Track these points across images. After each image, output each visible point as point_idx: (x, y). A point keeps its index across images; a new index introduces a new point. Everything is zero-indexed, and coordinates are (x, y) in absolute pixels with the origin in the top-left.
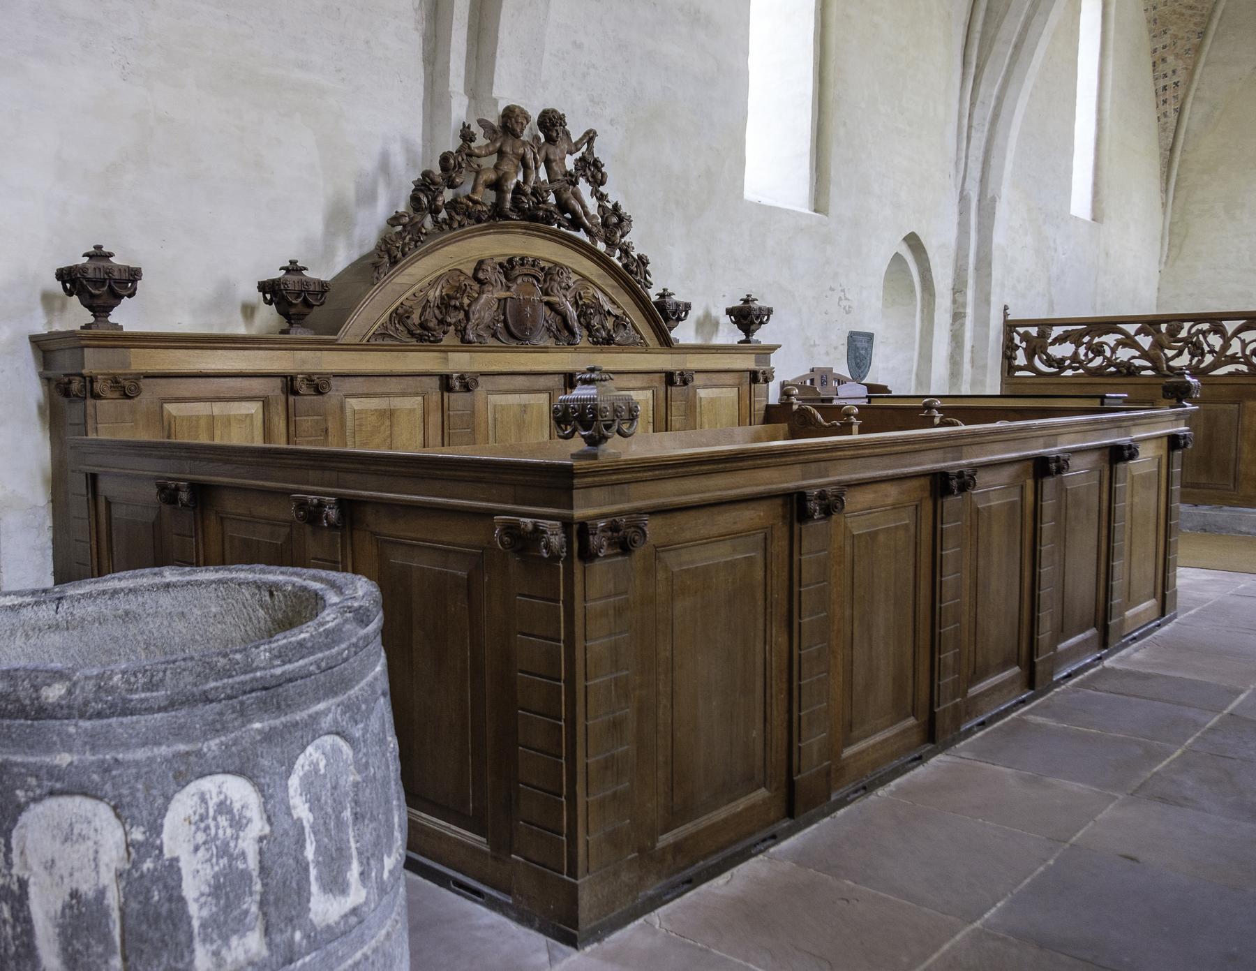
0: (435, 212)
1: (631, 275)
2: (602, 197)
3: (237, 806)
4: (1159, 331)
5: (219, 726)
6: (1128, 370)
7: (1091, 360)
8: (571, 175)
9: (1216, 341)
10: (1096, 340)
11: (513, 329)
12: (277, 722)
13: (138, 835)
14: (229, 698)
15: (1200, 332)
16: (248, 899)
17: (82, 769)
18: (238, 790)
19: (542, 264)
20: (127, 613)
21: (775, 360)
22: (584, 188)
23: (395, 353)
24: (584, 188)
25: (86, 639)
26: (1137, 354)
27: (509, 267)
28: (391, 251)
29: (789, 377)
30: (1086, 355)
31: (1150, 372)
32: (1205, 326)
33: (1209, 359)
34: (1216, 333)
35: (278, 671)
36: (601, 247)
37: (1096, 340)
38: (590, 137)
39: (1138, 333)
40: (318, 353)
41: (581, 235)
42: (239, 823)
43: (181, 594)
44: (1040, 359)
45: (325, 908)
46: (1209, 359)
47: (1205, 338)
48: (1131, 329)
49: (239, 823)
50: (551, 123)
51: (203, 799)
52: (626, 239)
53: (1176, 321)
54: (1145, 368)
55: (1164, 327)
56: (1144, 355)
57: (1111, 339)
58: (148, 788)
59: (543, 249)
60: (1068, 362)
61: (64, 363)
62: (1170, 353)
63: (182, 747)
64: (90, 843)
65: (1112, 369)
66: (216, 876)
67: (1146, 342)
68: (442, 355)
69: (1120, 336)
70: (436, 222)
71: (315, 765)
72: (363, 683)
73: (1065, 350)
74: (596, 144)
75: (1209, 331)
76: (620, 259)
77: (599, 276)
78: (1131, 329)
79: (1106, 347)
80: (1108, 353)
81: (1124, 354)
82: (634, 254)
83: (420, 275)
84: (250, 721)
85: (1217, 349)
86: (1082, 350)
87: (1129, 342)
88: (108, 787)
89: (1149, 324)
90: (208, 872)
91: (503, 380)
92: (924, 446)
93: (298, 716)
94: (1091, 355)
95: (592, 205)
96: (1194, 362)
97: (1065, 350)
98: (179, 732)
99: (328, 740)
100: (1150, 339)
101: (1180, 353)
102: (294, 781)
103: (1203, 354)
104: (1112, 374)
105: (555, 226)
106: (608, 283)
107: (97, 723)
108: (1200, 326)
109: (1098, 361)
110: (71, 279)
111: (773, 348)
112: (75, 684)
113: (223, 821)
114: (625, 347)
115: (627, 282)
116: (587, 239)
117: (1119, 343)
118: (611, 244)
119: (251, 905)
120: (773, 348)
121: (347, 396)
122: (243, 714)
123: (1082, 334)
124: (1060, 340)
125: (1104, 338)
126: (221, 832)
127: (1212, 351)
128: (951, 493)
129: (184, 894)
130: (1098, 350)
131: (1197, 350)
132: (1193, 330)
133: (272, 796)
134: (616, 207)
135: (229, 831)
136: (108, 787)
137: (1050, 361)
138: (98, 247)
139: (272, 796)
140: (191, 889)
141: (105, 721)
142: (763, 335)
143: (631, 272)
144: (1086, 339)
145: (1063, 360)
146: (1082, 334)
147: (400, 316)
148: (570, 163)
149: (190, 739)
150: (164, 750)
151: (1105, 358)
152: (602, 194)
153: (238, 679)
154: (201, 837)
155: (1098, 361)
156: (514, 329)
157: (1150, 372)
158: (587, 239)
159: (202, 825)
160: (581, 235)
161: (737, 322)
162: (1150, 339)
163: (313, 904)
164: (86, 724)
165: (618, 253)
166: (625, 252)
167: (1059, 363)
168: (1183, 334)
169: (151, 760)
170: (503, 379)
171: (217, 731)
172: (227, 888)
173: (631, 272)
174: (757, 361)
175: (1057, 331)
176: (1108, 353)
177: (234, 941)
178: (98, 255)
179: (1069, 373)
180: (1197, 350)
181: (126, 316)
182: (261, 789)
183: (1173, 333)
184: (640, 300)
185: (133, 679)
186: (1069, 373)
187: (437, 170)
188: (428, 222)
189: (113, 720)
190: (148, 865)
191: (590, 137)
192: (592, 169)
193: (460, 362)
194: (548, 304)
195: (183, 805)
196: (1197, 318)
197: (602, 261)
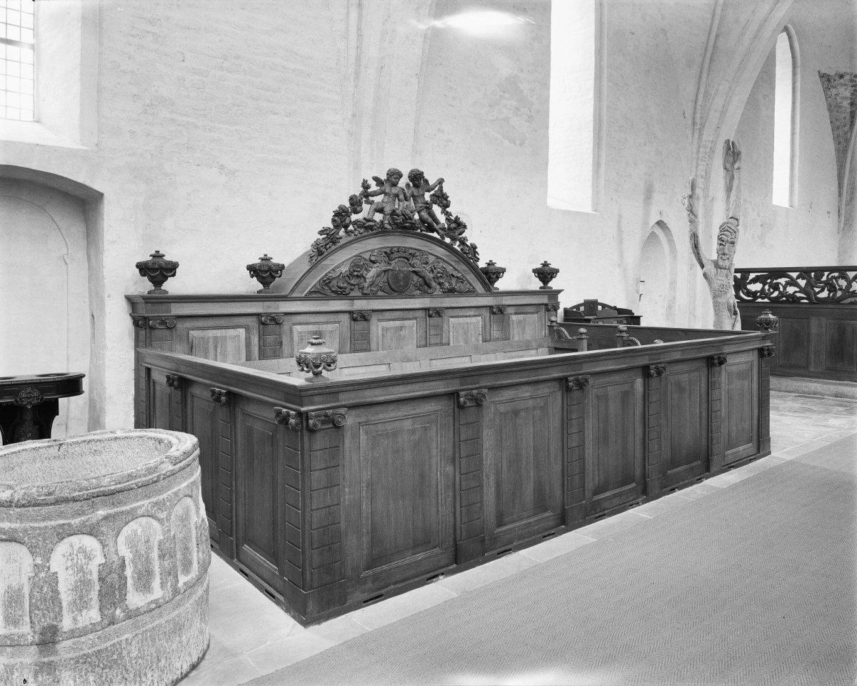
0: (346, 227)
1: (468, 254)
2: (448, 214)
3: (88, 549)
4: (810, 277)
5: (80, 512)
6: (793, 299)
7: (772, 293)
8: (427, 203)
9: (843, 283)
10: (775, 281)
11: (393, 287)
12: (112, 511)
13: (39, 561)
14: (85, 499)
15: (834, 277)
16: (92, 593)
17: (15, 530)
18: (90, 542)
19: (411, 251)
20: (95, 451)
21: (561, 297)
22: (437, 209)
23: (323, 302)
24: (437, 209)
25: (74, 463)
26: (798, 290)
27: (389, 254)
28: (320, 251)
29: (569, 306)
30: (769, 290)
31: (806, 301)
32: (836, 274)
33: (839, 294)
34: (843, 278)
35: (113, 488)
36: (448, 240)
37: (775, 281)
38: (441, 182)
39: (798, 278)
40: (277, 303)
41: (435, 235)
42: (89, 557)
43: (122, 442)
44: (742, 292)
45: (135, 599)
46: (839, 294)
47: (837, 281)
48: (794, 275)
49: (89, 557)
50: (417, 178)
51: (71, 546)
52: (463, 235)
53: (819, 271)
54: (803, 298)
55: (813, 274)
56: (802, 290)
57: (783, 281)
58: (44, 540)
59: (411, 243)
60: (759, 294)
61: (142, 311)
62: (817, 290)
63: (61, 522)
64: (18, 564)
65: (784, 299)
66: (76, 582)
67: (802, 283)
68: (350, 301)
69: (787, 279)
70: (347, 232)
71: (135, 532)
72: (169, 492)
73: (757, 287)
74: (444, 185)
75: (839, 277)
76: (459, 246)
77: (447, 256)
78: (794, 275)
79: (780, 286)
80: (781, 289)
81: (791, 290)
82: (468, 243)
83: (340, 261)
84: (97, 510)
85: (844, 288)
86: (767, 287)
87: (792, 283)
88: (26, 539)
89: (804, 272)
90: (73, 579)
91: (387, 315)
92: (540, 366)
93: (124, 508)
94: (772, 290)
95: (442, 218)
96: (831, 294)
97: (757, 287)
98: (61, 515)
99: (144, 520)
100: (805, 281)
101: (822, 290)
102: (121, 539)
103: (835, 290)
104: (783, 301)
105: (419, 231)
106: (452, 259)
107: (23, 509)
108: (833, 274)
109: (776, 294)
110: (143, 269)
111: (560, 291)
112: (15, 492)
113: (81, 556)
114: (462, 293)
115: (463, 258)
116: (438, 237)
117: (788, 284)
118: (454, 239)
119: (94, 595)
120: (560, 291)
121: (294, 324)
122: (94, 507)
123: (766, 277)
124: (754, 281)
125: (779, 280)
126: (79, 561)
127: (841, 289)
128: (652, 376)
129: (58, 589)
130: (776, 287)
131: (832, 289)
132: (830, 277)
133: (107, 545)
134: (457, 218)
135: (83, 561)
136: (26, 539)
137: (749, 293)
138: (157, 252)
139: (107, 545)
140: (62, 587)
141: (27, 509)
142: (554, 284)
143: (466, 253)
144: (769, 281)
145: (756, 292)
146: (766, 277)
147: (326, 282)
148: (427, 196)
149: (66, 518)
150: (53, 523)
151: (780, 292)
152: (447, 212)
153: (90, 491)
154: (69, 563)
155: (776, 294)
156: (396, 287)
157: (806, 301)
158: (438, 237)
159: (70, 558)
160: (435, 235)
161: (539, 277)
162: (805, 281)
163: (129, 596)
164: (19, 510)
165: (458, 243)
166: (463, 242)
167: (754, 294)
168: (824, 278)
169: (46, 527)
170: (387, 313)
171: (80, 515)
172: (82, 586)
173: (466, 253)
174: (549, 299)
175: (752, 276)
176: (781, 289)
177: (84, 612)
178: (157, 256)
179: (759, 300)
180: (832, 289)
181: (172, 286)
182: (104, 546)
183: (818, 278)
184: (474, 269)
185: (41, 490)
186: (759, 300)
187: (348, 205)
188: (342, 232)
189: (30, 509)
190: (42, 575)
191: (441, 182)
192: (442, 200)
193: (360, 305)
194: (414, 272)
195: (62, 548)
196: (832, 270)
197: (449, 248)
